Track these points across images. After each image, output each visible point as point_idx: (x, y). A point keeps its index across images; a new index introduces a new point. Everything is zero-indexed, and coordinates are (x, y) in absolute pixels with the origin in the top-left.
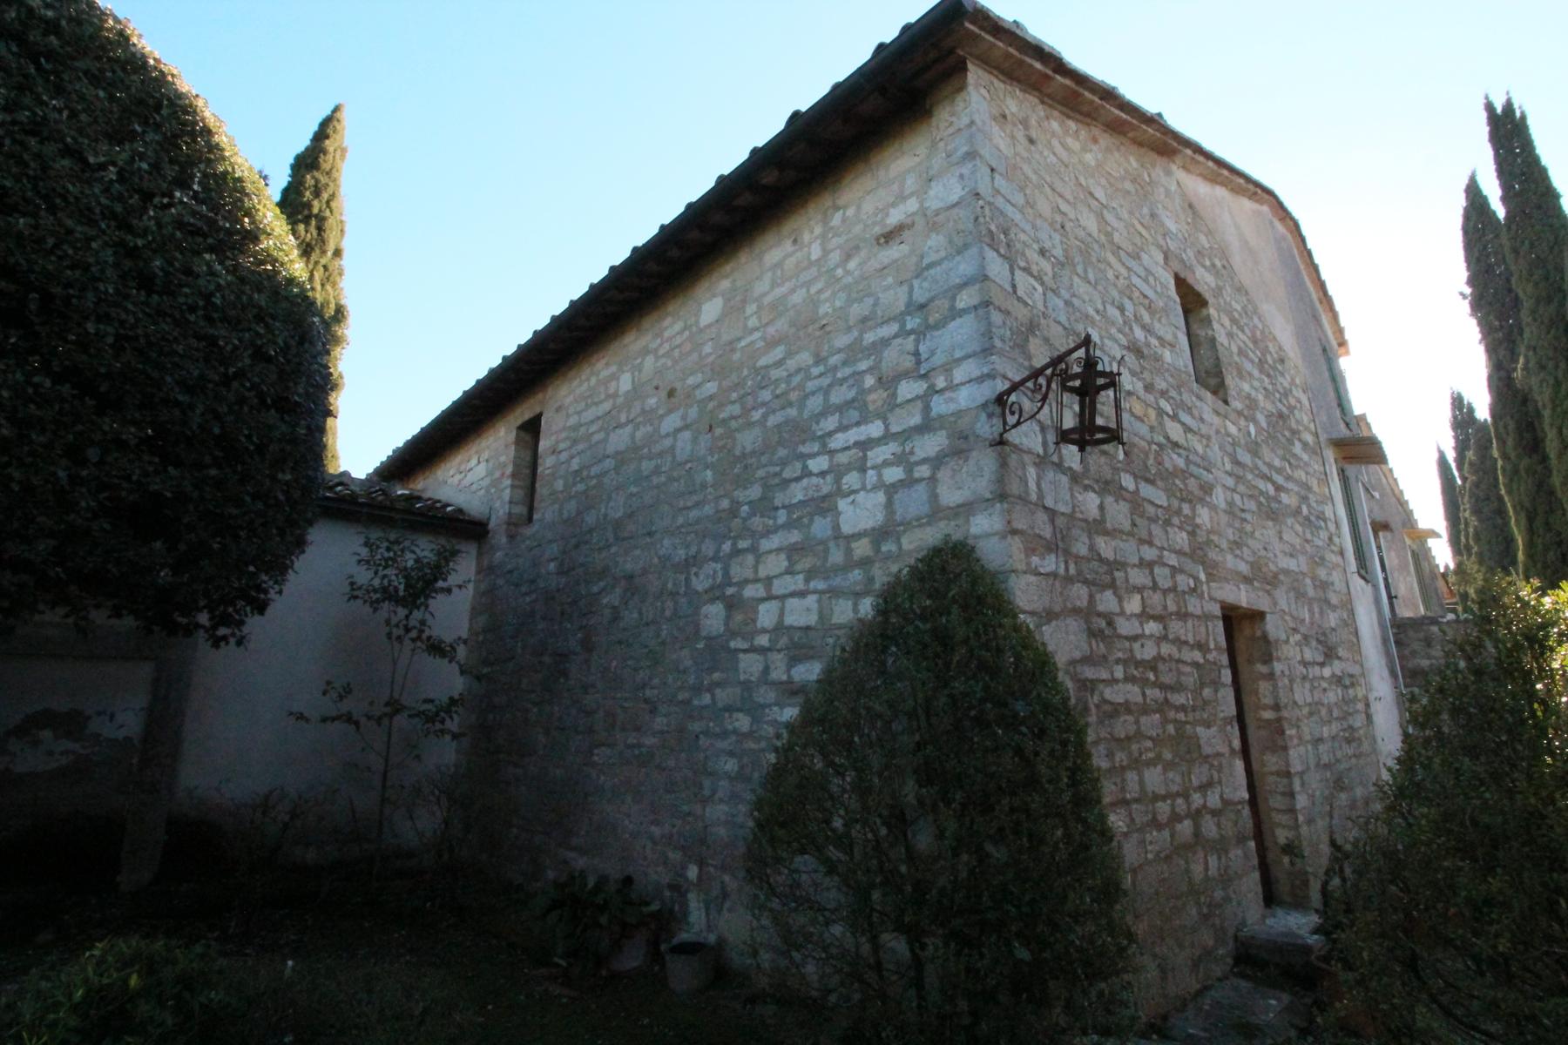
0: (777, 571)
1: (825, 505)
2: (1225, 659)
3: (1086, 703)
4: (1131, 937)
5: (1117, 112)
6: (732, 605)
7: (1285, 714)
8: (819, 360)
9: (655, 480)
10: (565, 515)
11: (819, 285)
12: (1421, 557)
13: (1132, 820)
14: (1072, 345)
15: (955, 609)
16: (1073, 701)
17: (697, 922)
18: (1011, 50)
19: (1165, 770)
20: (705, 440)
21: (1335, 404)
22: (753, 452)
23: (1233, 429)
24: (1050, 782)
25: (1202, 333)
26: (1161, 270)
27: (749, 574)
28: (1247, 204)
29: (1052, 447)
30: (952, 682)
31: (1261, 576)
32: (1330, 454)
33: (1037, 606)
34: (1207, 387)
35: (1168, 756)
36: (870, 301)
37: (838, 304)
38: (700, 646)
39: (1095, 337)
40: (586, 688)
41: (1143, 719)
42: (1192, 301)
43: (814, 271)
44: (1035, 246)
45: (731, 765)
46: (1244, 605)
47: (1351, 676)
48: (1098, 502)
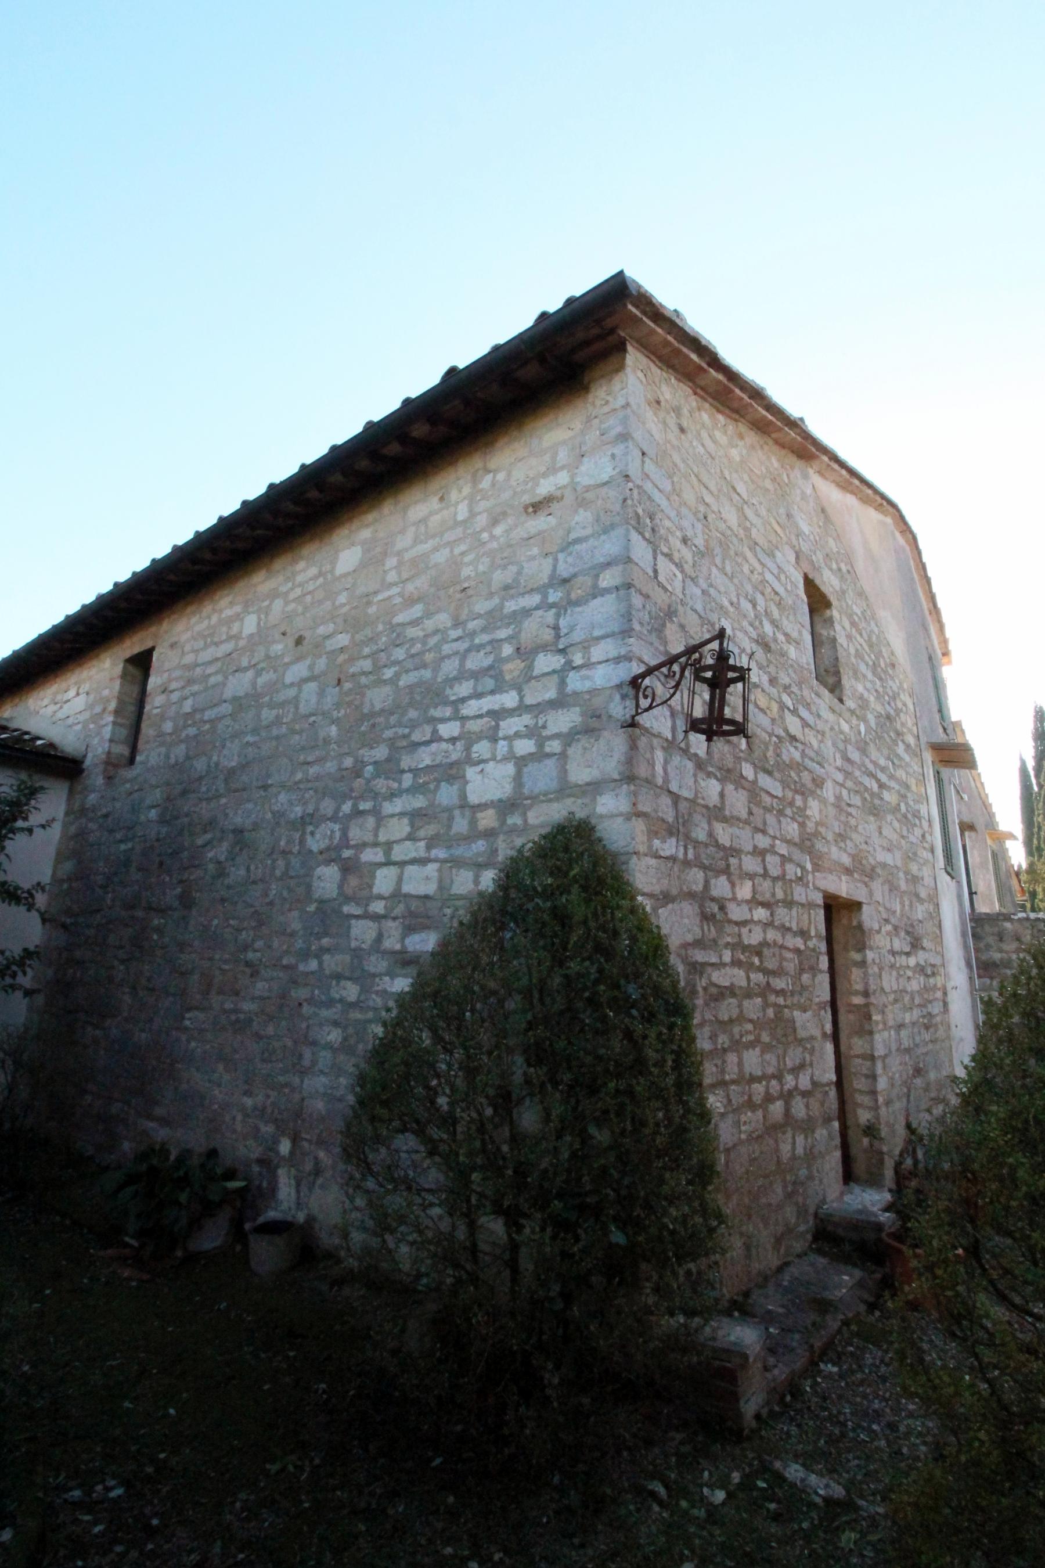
0: (398, 836)
1: (454, 771)
2: (823, 947)
3: (694, 986)
4: (720, 1217)
5: (764, 413)
6: (348, 868)
7: (873, 1000)
8: (457, 624)
9: (275, 732)
10: (172, 761)
11: (463, 548)
12: (999, 857)
13: (730, 1101)
14: (707, 636)
15: (575, 889)
16: (682, 984)
17: (286, 1198)
18: (670, 338)
19: (763, 1052)
20: (332, 694)
21: (935, 709)
22: (383, 710)
23: (845, 727)
24: (655, 1065)
25: (824, 633)
26: (792, 569)
27: (369, 837)
28: (873, 515)
29: (681, 736)
30: (567, 970)
31: (861, 869)
32: (928, 756)
33: (657, 889)
34: (824, 684)
35: (765, 1038)
36: (513, 569)
37: (481, 568)
38: (312, 908)
39: (729, 632)
40: (182, 946)
41: (746, 1003)
42: (818, 601)
43: (459, 531)
44: (678, 534)
45: (334, 1036)
46: (844, 895)
47: (933, 966)
48: (719, 788)
